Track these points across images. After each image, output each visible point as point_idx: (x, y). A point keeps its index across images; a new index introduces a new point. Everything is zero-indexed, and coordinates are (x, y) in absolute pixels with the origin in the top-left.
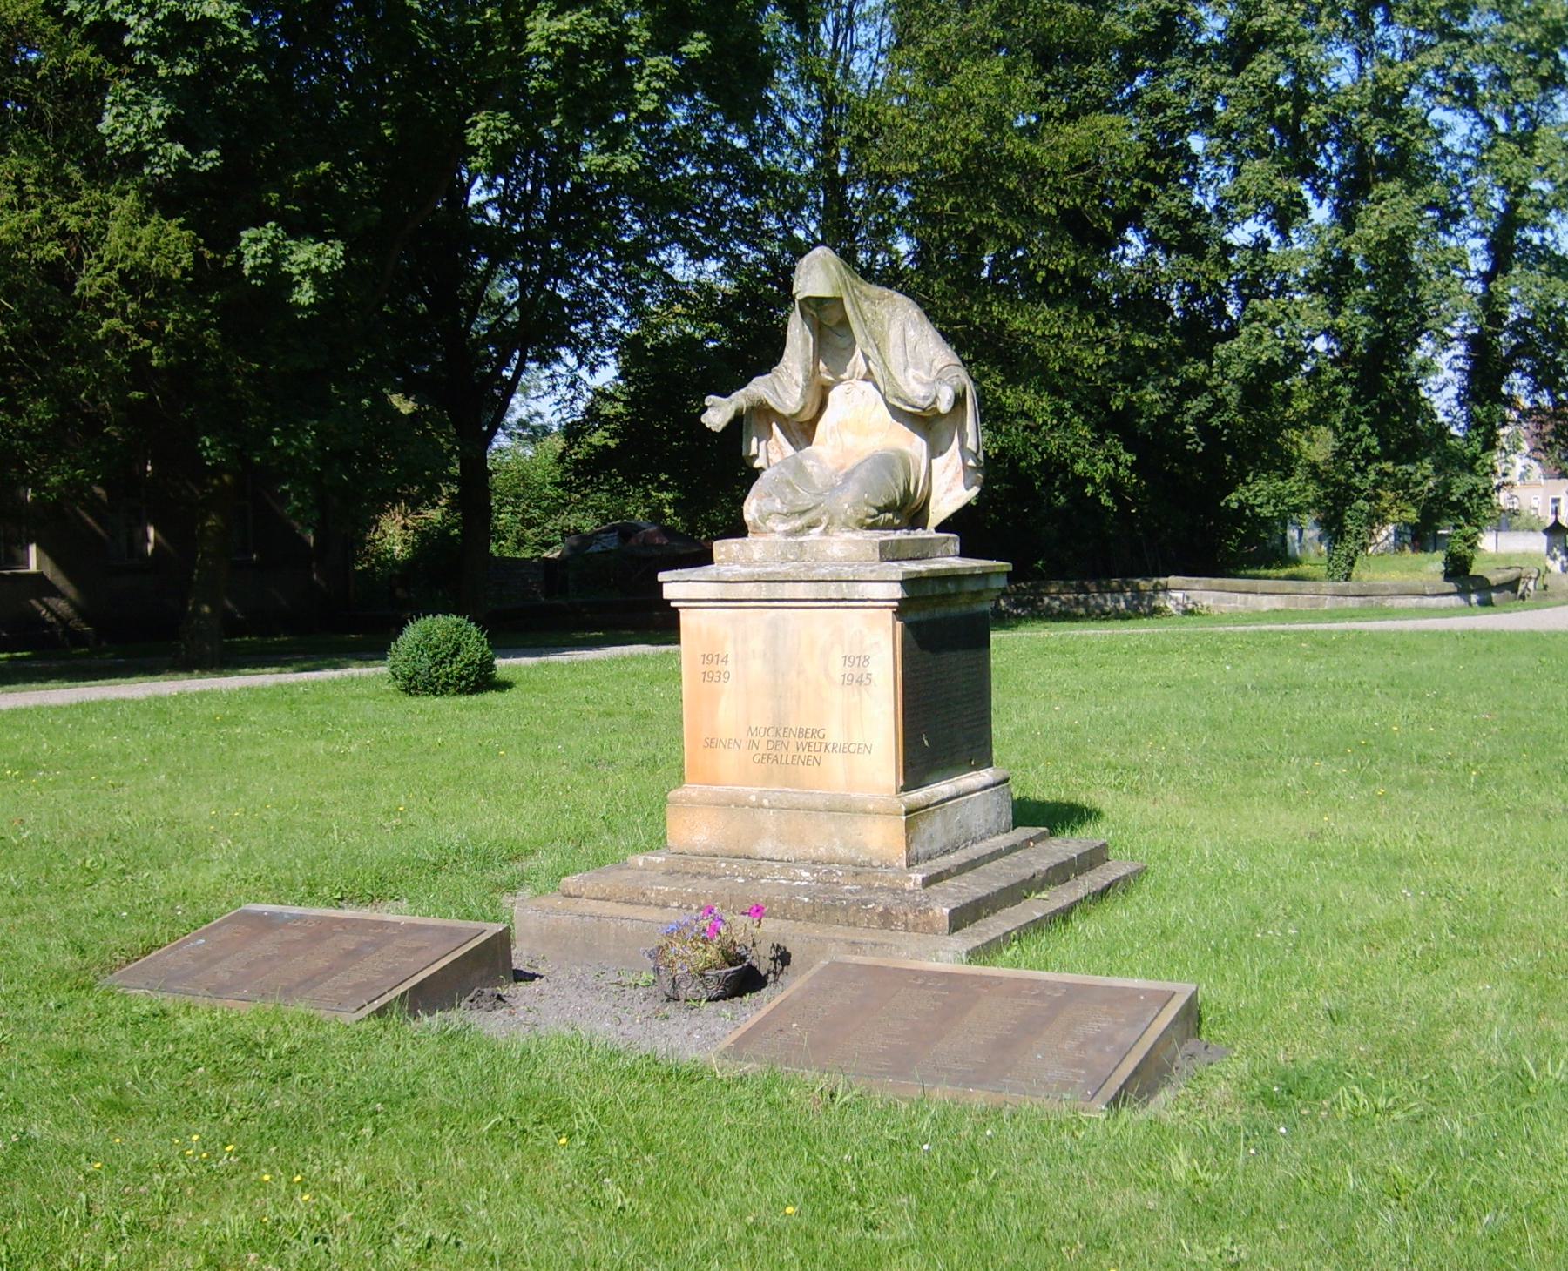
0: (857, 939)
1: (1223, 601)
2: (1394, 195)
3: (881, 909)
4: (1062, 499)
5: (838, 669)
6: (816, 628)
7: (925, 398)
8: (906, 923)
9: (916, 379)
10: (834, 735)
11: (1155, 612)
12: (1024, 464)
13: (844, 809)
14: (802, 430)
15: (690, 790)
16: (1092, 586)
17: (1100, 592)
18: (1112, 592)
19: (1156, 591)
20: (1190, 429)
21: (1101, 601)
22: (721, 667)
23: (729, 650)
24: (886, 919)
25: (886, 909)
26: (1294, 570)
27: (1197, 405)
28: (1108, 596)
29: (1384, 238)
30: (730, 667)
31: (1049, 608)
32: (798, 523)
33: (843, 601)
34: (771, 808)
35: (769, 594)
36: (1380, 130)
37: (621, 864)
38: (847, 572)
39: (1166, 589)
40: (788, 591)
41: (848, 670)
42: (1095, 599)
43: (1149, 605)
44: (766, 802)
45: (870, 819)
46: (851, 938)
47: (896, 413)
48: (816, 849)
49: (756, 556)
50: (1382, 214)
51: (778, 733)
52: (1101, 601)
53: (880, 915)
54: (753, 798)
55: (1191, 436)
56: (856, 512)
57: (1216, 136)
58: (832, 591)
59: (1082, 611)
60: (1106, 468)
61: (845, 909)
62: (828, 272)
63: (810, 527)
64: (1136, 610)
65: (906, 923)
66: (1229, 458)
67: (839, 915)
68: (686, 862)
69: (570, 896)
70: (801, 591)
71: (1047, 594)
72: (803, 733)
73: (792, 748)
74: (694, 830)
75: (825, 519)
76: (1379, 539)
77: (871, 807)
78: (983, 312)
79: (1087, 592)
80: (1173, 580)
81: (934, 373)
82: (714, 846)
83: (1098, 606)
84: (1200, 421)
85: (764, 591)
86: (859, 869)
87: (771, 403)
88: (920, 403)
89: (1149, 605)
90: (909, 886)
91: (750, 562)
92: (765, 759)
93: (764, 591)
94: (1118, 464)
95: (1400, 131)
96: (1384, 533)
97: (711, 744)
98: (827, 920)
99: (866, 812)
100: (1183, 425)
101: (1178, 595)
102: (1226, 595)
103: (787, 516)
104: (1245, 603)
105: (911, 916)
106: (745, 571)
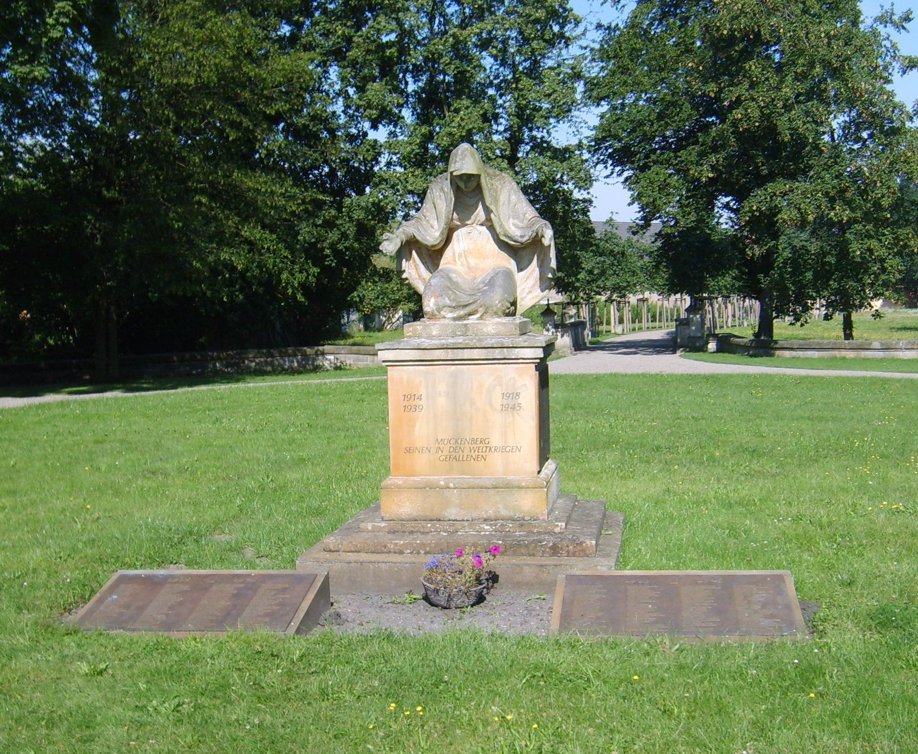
0: (544, 563)
1: (358, 360)
2: (467, 108)
3: (551, 544)
4: (241, 297)
5: (498, 401)
6: (484, 378)
7: (521, 237)
8: (568, 552)
9: (515, 225)
10: (496, 441)
11: (316, 369)
12: (248, 274)
13: (506, 487)
14: (432, 256)
15: (393, 480)
16: (276, 353)
17: (281, 357)
18: (289, 356)
19: (317, 355)
20: (328, 251)
21: (281, 362)
22: (417, 402)
23: (423, 391)
24: (555, 550)
25: (554, 544)
26: (351, 341)
27: (333, 236)
28: (286, 359)
29: (464, 134)
30: (423, 402)
31: (248, 367)
32: (462, 312)
33: (505, 360)
34: (455, 488)
35: (454, 355)
36: (457, 68)
37: (359, 530)
38: (507, 342)
39: (323, 354)
40: (466, 354)
41: (505, 402)
42: (278, 361)
43: (313, 364)
44: (451, 485)
45: (523, 491)
46: (539, 563)
47: (504, 246)
48: (487, 512)
49: (434, 333)
50: (462, 119)
51: (457, 442)
52: (281, 362)
53: (551, 548)
54: (442, 483)
55: (328, 256)
56: (502, 306)
57: (348, 67)
58: (497, 354)
59: (269, 368)
60: (300, 277)
61: (527, 546)
62: (475, 159)
63: (470, 315)
64: (304, 367)
65: (568, 552)
66: (345, 270)
67: (523, 550)
68: (402, 525)
69: (331, 551)
70: (475, 354)
71: (248, 358)
72: (474, 441)
73: (467, 452)
74: (401, 505)
75: (481, 310)
76: (394, 320)
77: (524, 484)
78: (225, 176)
79: (273, 356)
80: (327, 348)
81: (526, 222)
82: (415, 514)
83: (280, 365)
84: (332, 246)
85: (450, 354)
86: (521, 522)
87: (419, 238)
88: (520, 239)
89: (313, 364)
90: (557, 530)
91: (430, 337)
92: (448, 458)
93: (450, 354)
94: (309, 275)
95: (469, 69)
96: (397, 316)
97: (409, 450)
98: (515, 554)
99: (519, 487)
100: (323, 249)
101: (331, 357)
102: (361, 357)
103: (455, 308)
104: (373, 361)
105: (571, 547)
106: (435, 342)
